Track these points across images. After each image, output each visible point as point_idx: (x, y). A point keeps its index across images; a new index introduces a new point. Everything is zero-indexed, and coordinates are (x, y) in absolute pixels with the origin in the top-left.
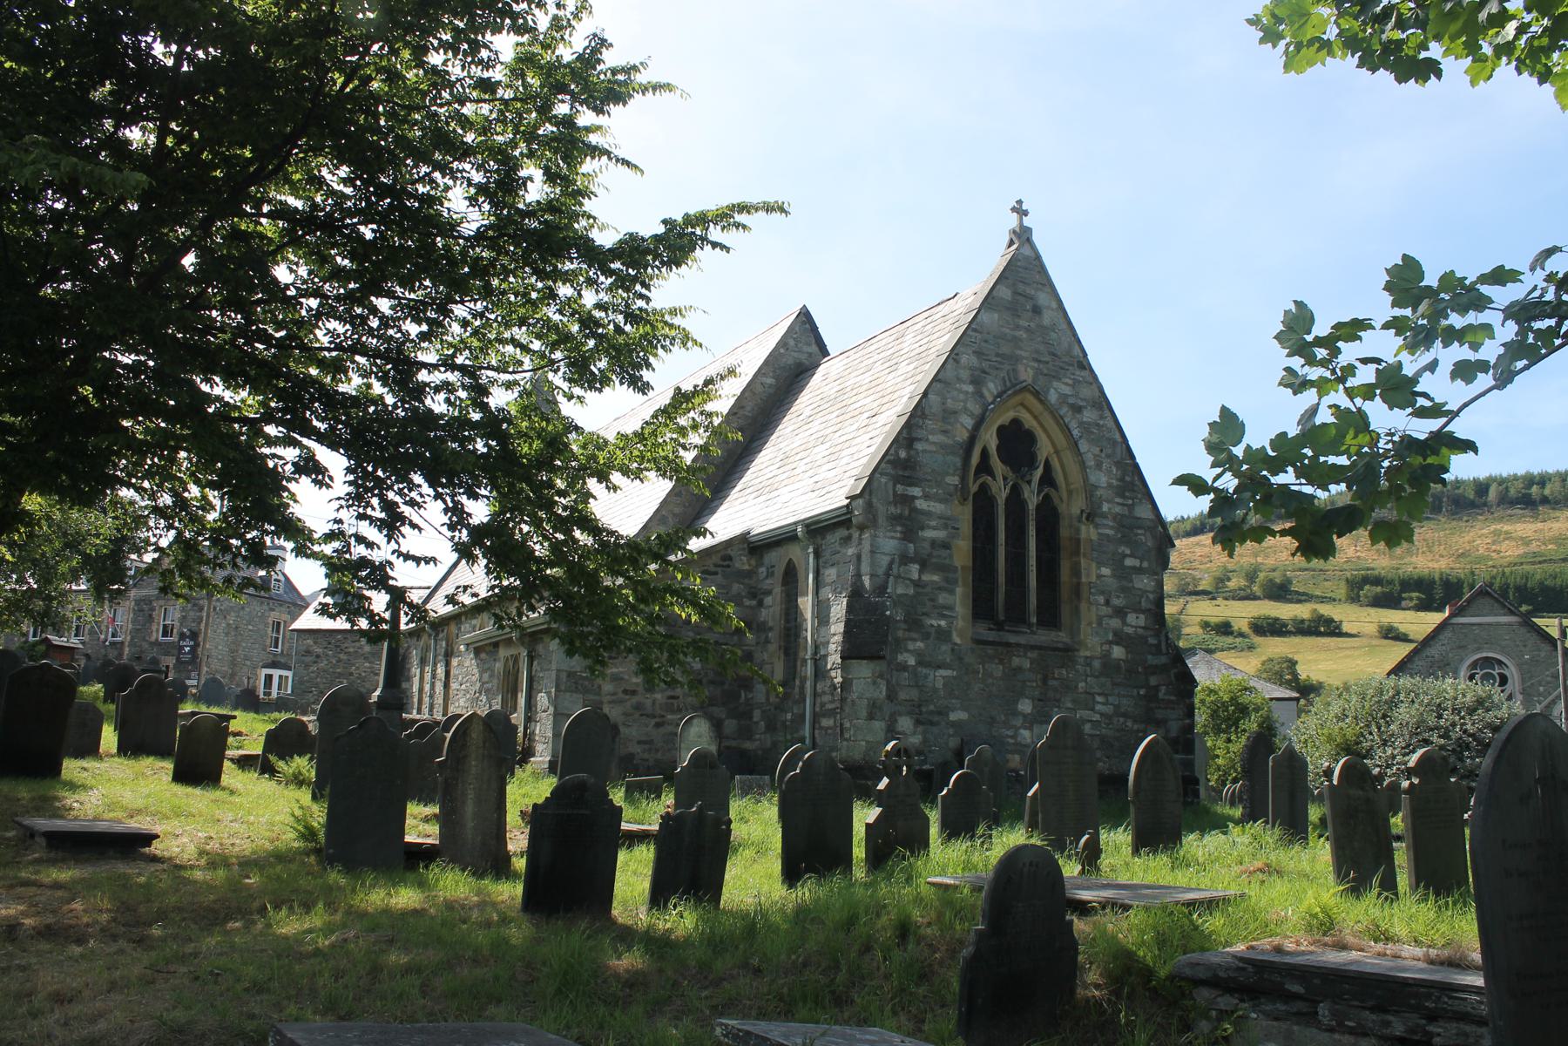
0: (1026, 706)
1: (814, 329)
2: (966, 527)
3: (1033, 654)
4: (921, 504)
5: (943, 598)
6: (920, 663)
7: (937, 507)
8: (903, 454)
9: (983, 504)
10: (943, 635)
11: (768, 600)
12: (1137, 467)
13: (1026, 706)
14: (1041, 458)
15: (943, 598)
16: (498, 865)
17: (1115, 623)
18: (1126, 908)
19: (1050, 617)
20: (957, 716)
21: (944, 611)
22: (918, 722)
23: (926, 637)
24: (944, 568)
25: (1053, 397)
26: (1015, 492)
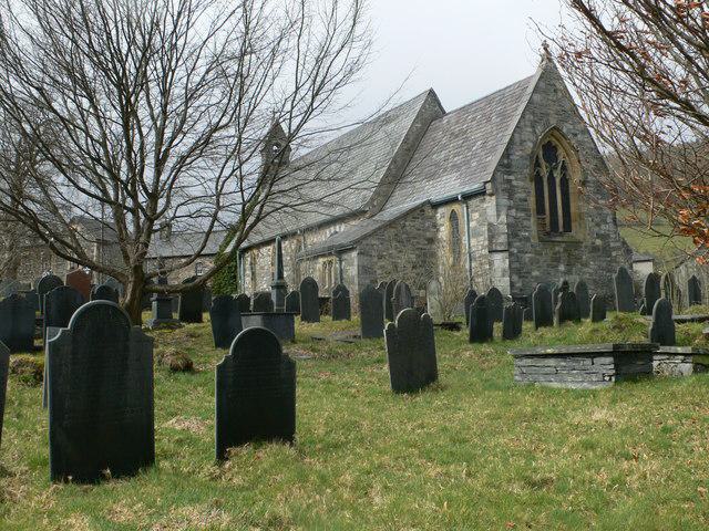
0: (562, 268)
1: (435, 95)
2: (533, 192)
3: (564, 245)
4: (514, 183)
5: (525, 223)
6: (519, 252)
7: (521, 184)
8: (506, 161)
9: (538, 180)
10: (527, 239)
11: (442, 229)
12: (488, 99)
13: (562, 268)
14: (561, 159)
15: (525, 223)
16: (382, 348)
17: (597, 229)
18: (516, 357)
19: (568, 228)
20: (535, 273)
21: (526, 228)
22: (520, 277)
23: (520, 240)
24: (524, 210)
25: (564, 130)
26: (551, 174)
